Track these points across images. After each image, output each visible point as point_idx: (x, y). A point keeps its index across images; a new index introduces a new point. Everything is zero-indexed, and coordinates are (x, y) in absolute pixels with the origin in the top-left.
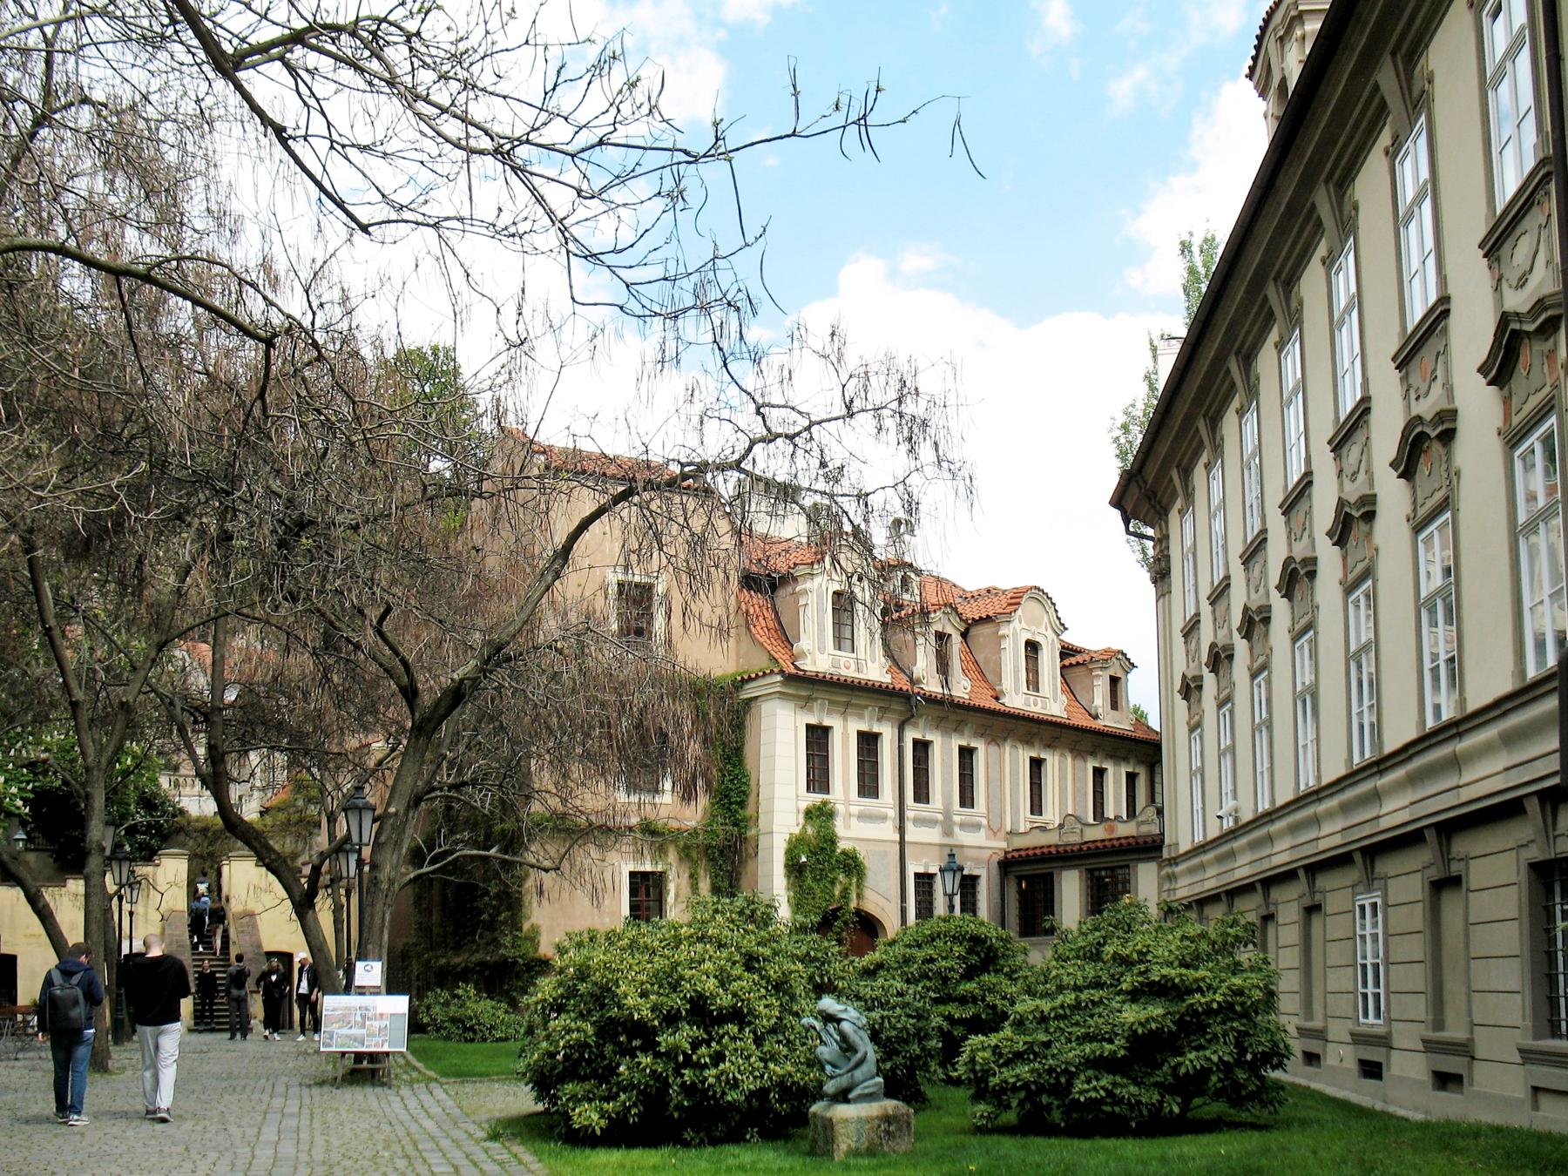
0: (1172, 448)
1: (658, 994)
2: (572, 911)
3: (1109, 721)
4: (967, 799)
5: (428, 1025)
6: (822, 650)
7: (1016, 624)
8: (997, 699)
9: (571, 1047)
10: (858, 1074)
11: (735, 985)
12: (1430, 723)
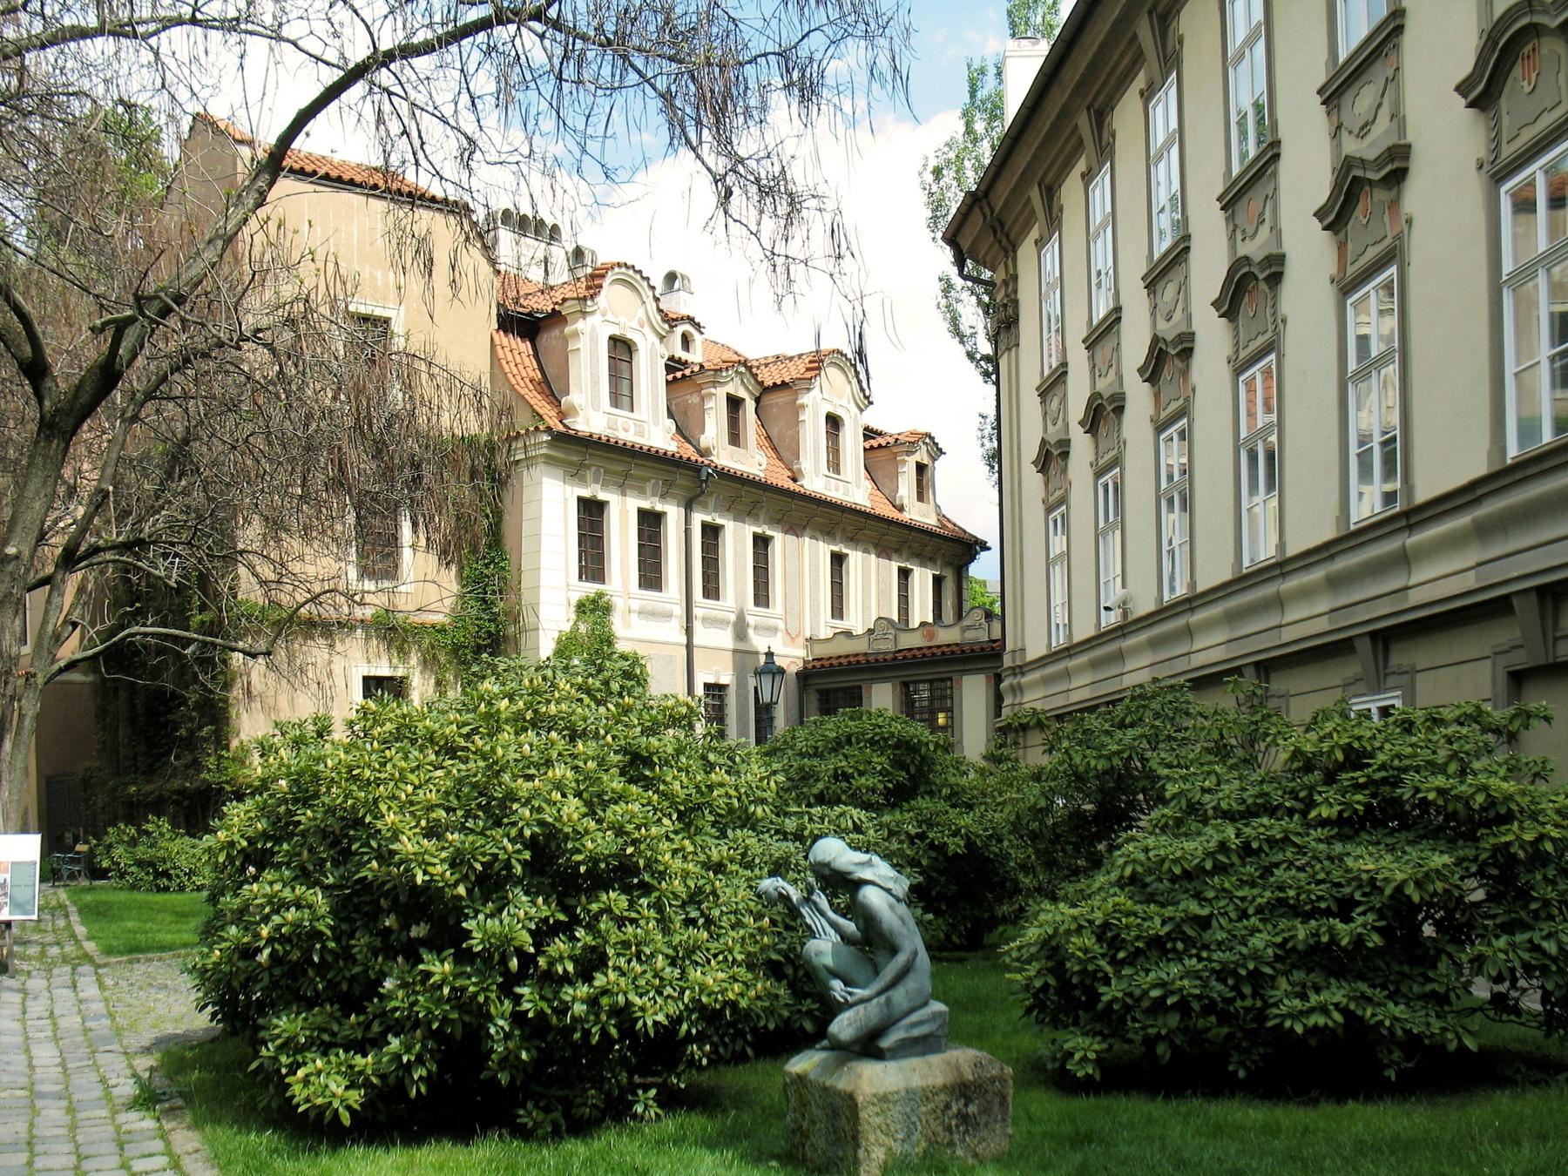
0: (1035, 157)
1: (463, 828)
2: (295, 705)
3: (918, 514)
4: (762, 596)
5: (108, 870)
6: (596, 406)
7: (815, 392)
8: (794, 480)
9: (283, 939)
10: (900, 996)
11: (615, 812)
12: (1513, 451)
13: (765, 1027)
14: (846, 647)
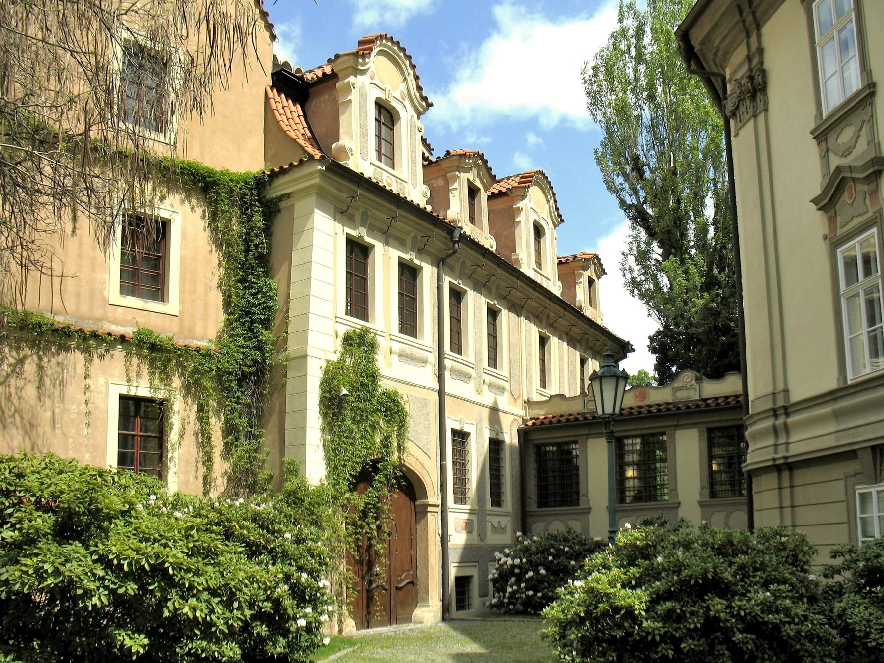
4: (493, 361)
13: (144, 646)
14: (564, 409)
